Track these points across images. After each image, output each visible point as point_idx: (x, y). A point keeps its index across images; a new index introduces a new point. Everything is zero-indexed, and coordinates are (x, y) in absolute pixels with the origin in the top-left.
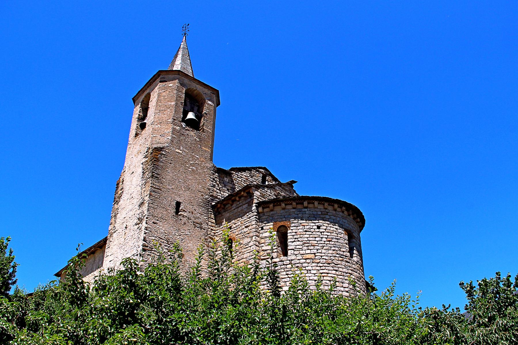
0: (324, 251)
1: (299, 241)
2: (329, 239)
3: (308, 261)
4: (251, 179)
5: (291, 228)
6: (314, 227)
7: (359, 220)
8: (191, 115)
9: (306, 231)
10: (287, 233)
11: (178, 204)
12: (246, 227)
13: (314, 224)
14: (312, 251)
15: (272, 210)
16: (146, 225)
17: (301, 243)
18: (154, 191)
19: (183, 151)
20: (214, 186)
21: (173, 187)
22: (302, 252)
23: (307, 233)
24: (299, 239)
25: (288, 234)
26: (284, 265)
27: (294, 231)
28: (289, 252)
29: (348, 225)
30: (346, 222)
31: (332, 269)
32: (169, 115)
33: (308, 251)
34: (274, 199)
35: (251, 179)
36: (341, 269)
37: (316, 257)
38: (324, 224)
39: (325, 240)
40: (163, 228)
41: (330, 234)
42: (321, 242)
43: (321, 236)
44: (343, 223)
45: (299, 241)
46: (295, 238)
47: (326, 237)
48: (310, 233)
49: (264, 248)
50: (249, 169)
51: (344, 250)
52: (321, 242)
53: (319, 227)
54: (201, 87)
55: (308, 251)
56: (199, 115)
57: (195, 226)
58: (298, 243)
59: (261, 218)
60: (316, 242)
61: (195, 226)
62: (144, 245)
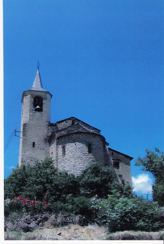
0: (77, 153)
3: (71, 158)
4: (66, 124)
8: (38, 107)
11: (34, 143)
15: (61, 140)
16: (22, 154)
18: (24, 141)
19: (35, 122)
20: (48, 132)
21: (31, 137)
22: (69, 155)
31: (80, 159)
32: (28, 108)
35: (66, 124)
36: (83, 159)
38: (77, 143)
40: (28, 153)
49: (59, 155)
50: (65, 120)
51: (85, 151)
53: (75, 144)
54: (41, 93)
56: (41, 106)
57: (41, 149)
59: (58, 144)
61: (41, 149)
62: (22, 161)
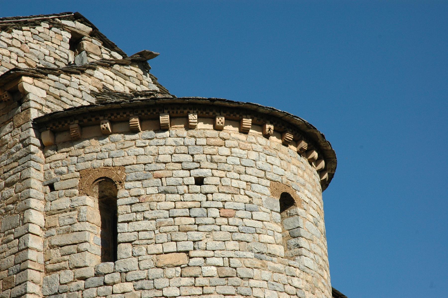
1: (145, 218)
2: (226, 213)
3: (170, 272)
5: (127, 185)
6: (186, 181)
7: (315, 154)
9: (166, 192)
10: (116, 198)
12: (8, 185)
13: (187, 173)
14: (182, 246)
17: (152, 225)
23: (169, 196)
24: (147, 215)
25: (119, 202)
26: (105, 284)
27: (134, 192)
28: (121, 247)
29: (281, 171)
30: (277, 161)
33: (172, 247)
34: (92, 105)
37: (192, 261)
39: (215, 213)
41: (229, 197)
42: (206, 220)
43: (206, 204)
44: (266, 167)
45: (145, 218)
46: (137, 212)
47: (220, 205)
48: (177, 197)
52: (206, 220)
55: (172, 247)
58: (144, 224)
60: (192, 220)
